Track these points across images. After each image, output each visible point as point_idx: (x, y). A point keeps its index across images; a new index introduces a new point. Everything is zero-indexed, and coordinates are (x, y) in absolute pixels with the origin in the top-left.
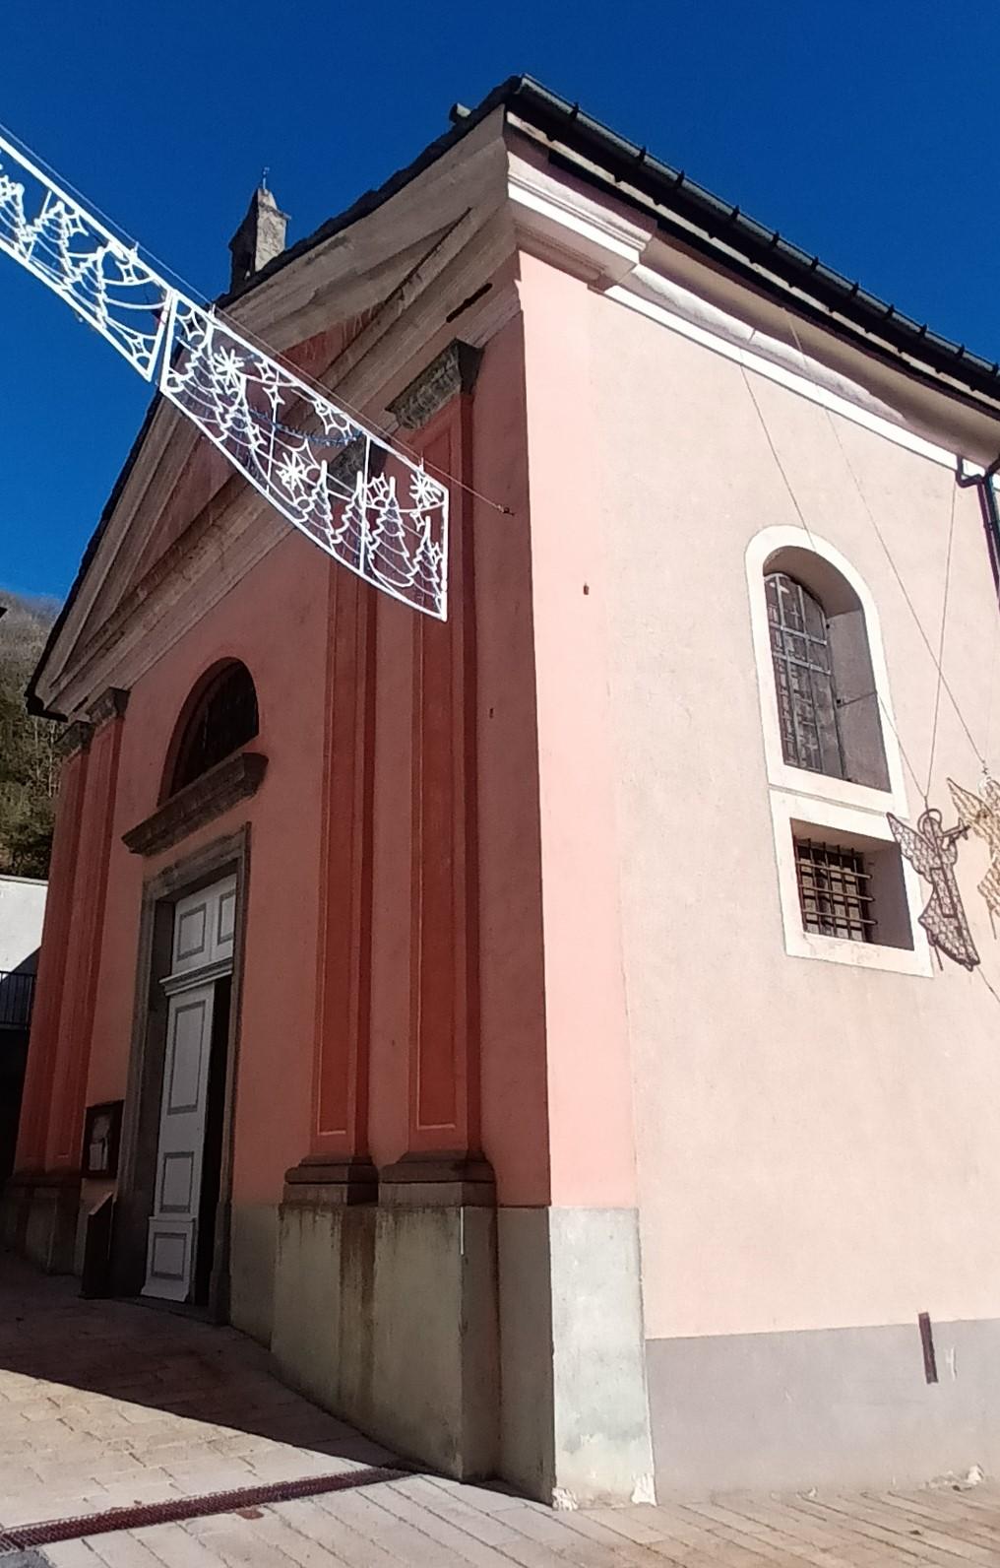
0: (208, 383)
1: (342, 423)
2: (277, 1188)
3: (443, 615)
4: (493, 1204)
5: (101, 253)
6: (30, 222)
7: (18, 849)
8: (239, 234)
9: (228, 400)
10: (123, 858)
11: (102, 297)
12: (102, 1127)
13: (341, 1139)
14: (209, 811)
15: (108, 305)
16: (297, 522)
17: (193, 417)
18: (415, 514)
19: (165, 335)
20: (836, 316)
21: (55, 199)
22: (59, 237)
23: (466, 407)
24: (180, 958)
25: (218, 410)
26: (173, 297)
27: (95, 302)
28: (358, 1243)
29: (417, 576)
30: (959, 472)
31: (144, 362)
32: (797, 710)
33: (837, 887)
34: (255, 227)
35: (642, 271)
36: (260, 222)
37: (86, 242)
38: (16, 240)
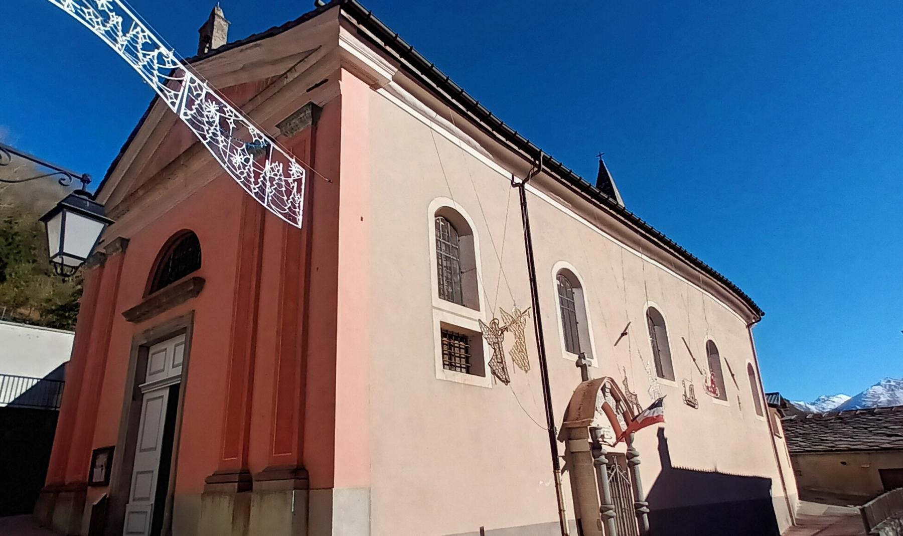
0: (202, 116)
1: (261, 138)
2: (201, 486)
3: (300, 226)
4: (307, 488)
5: (156, 52)
6: (124, 35)
7: (46, 312)
8: (204, 26)
9: (210, 124)
10: (121, 324)
11: (156, 73)
12: (102, 459)
13: (236, 462)
14: (172, 303)
15: (158, 77)
16: (238, 181)
17: (194, 131)
18: (290, 180)
19: (183, 92)
20: (469, 113)
21: (137, 25)
22: (137, 43)
23: (314, 135)
24: (150, 374)
25: (206, 128)
26: (188, 75)
27: (152, 74)
28: (242, 511)
29: (289, 208)
30: (512, 181)
31: (173, 104)
32: (445, 274)
33: (457, 350)
34: (213, 25)
35: (393, 84)
36: (216, 23)
37: (149, 47)
38: (117, 42)
